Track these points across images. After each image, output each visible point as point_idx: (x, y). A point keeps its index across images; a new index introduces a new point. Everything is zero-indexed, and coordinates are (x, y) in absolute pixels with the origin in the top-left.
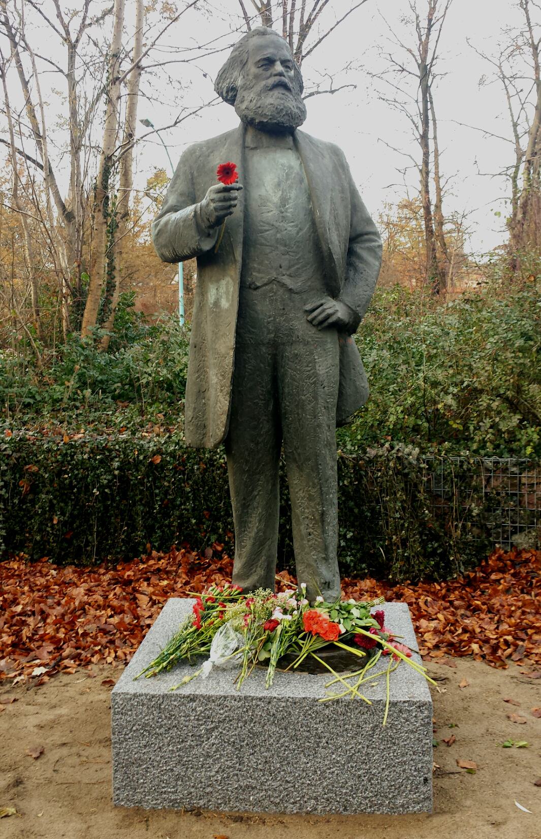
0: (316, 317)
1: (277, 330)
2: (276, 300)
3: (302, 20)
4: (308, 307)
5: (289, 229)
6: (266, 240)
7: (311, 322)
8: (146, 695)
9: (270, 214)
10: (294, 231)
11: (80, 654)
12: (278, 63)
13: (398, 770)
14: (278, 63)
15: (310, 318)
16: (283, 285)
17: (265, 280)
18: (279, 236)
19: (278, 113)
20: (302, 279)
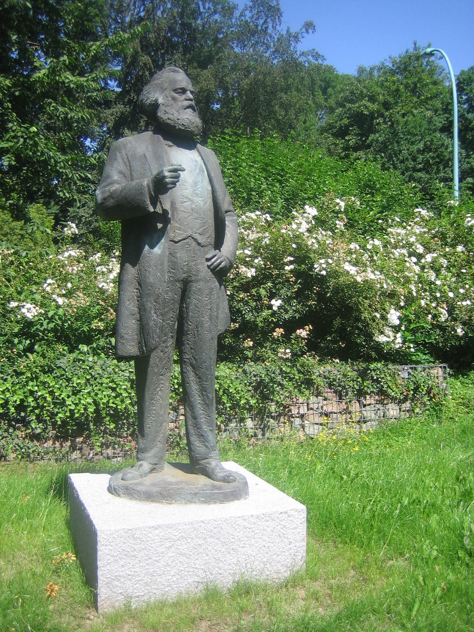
0: (213, 263)
1: (189, 271)
2: (190, 250)
3: (136, 484)
4: (209, 256)
5: (199, 202)
6: (185, 208)
7: (209, 267)
8: (124, 529)
9: (187, 191)
10: (202, 203)
11: (320, 87)
12: (188, 92)
13: (287, 554)
14: (188, 92)
15: (209, 263)
16: (195, 240)
17: (184, 236)
18: (193, 206)
19: (191, 125)
20: (206, 236)
